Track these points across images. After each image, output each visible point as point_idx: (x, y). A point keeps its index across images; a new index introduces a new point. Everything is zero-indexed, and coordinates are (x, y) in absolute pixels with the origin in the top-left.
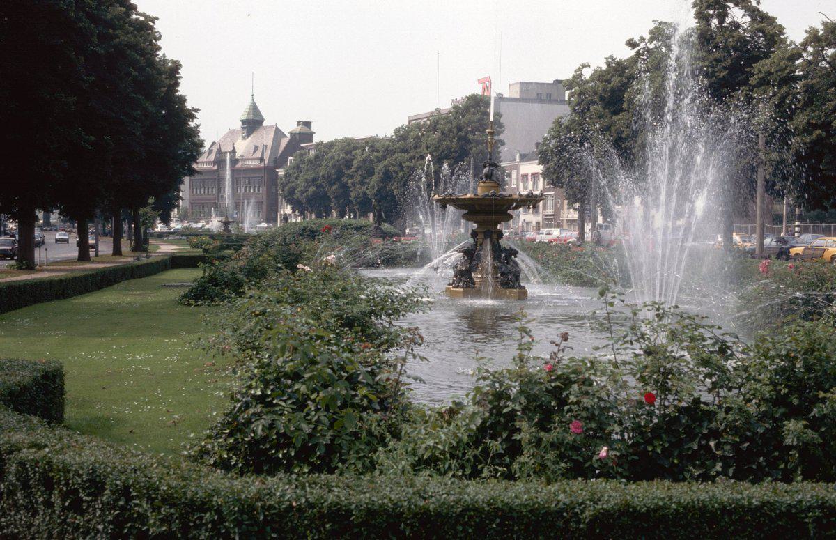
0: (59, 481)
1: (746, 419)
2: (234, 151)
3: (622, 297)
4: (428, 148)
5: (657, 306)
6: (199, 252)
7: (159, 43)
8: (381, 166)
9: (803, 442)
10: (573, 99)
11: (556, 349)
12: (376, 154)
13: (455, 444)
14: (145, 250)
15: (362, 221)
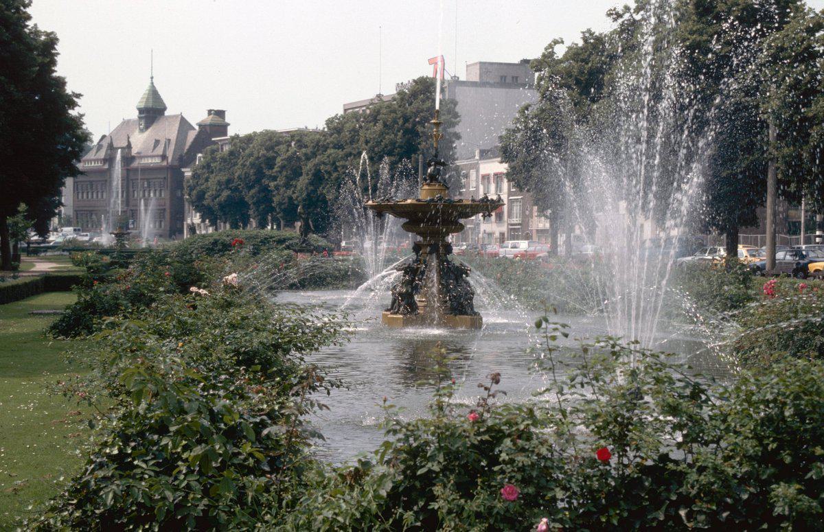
1: (723, 481)
2: (129, 146)
3: (566, 331)
4: (367, 142)
5: (611, 342)
6: (80, 271)
7: (29, 10)
8: (310, 165)
9: (797, 512)
11: (485, 394)
12: (304, 150)
15: (286, 233)
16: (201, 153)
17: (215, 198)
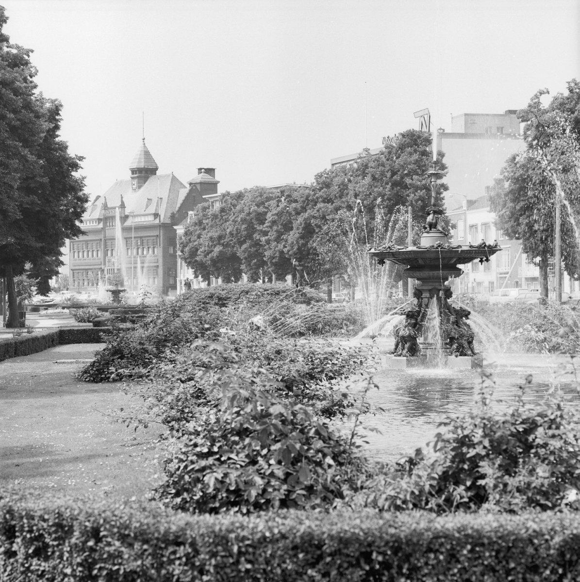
0: (22, 530)
2: (123, 206)
6: (89, 326)
8: (300, 219)
10: (529, 133)
12: (294, 205)
13: (417, 493)
14: (22, 325)
15: (278, 285)
16: (193, 210)
17: (208, 254)
